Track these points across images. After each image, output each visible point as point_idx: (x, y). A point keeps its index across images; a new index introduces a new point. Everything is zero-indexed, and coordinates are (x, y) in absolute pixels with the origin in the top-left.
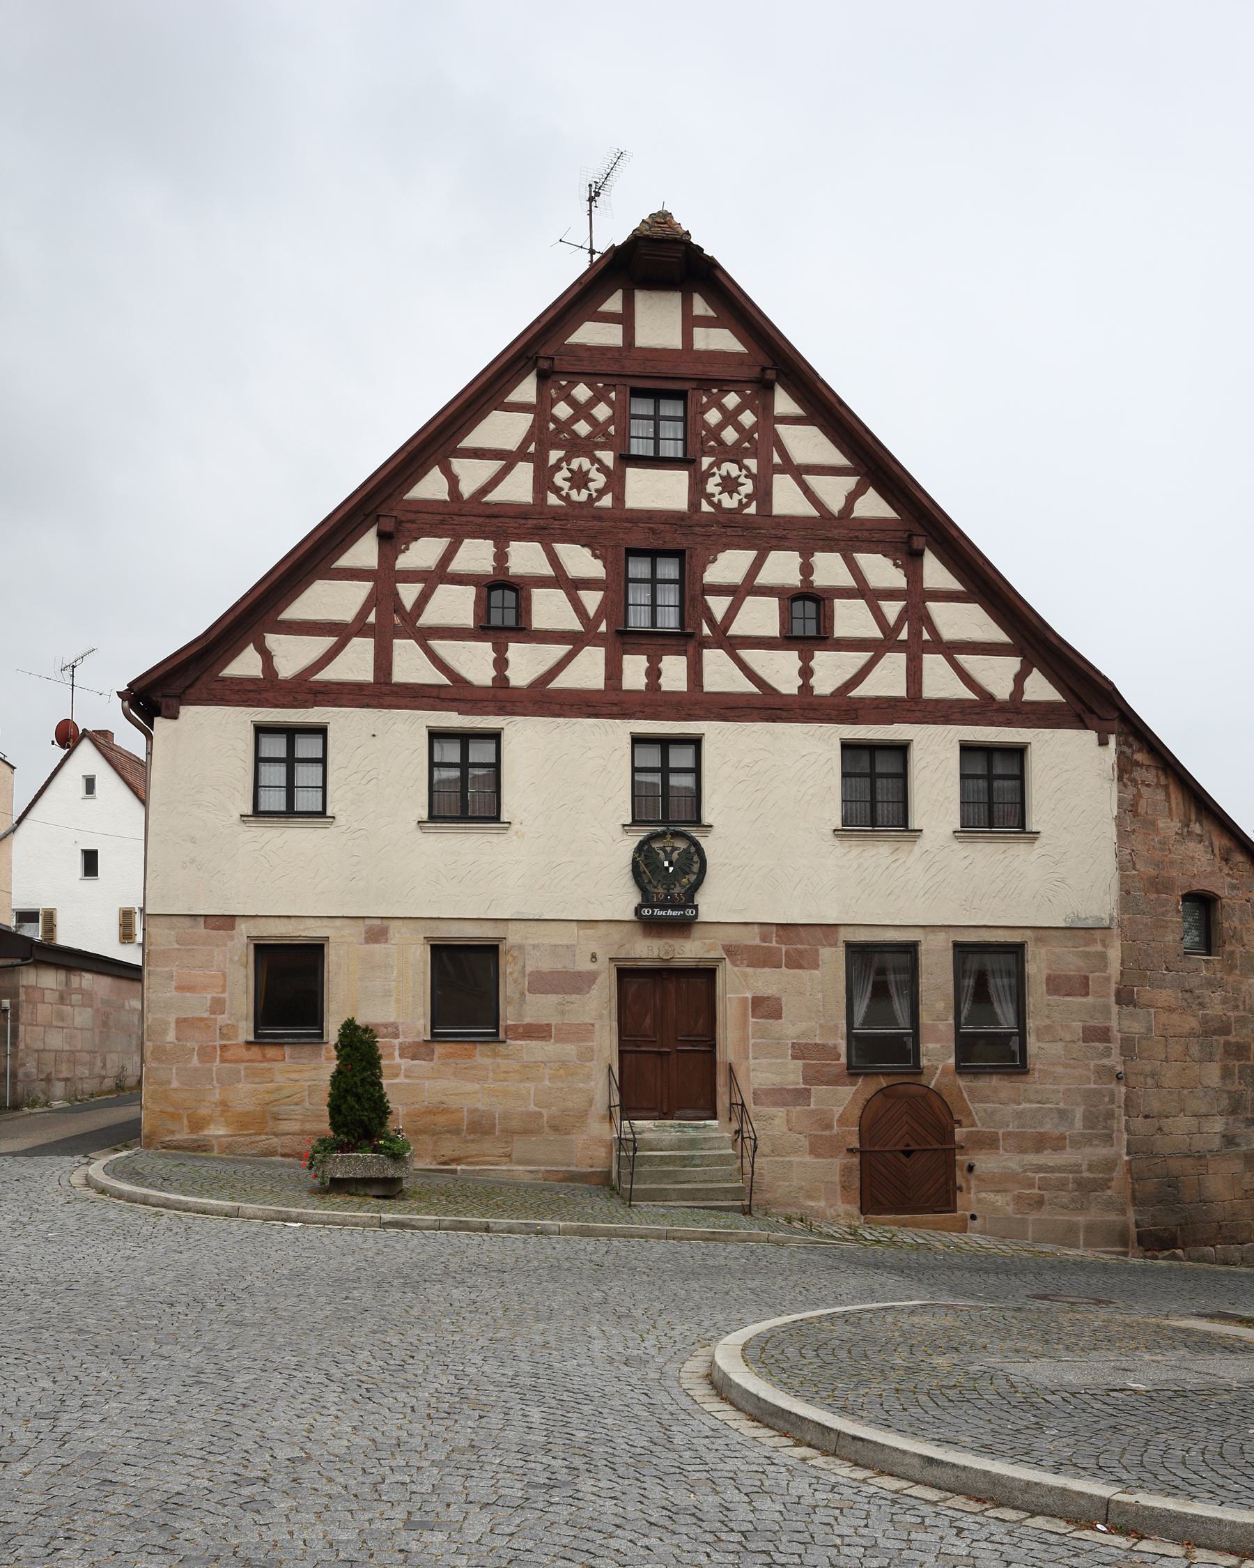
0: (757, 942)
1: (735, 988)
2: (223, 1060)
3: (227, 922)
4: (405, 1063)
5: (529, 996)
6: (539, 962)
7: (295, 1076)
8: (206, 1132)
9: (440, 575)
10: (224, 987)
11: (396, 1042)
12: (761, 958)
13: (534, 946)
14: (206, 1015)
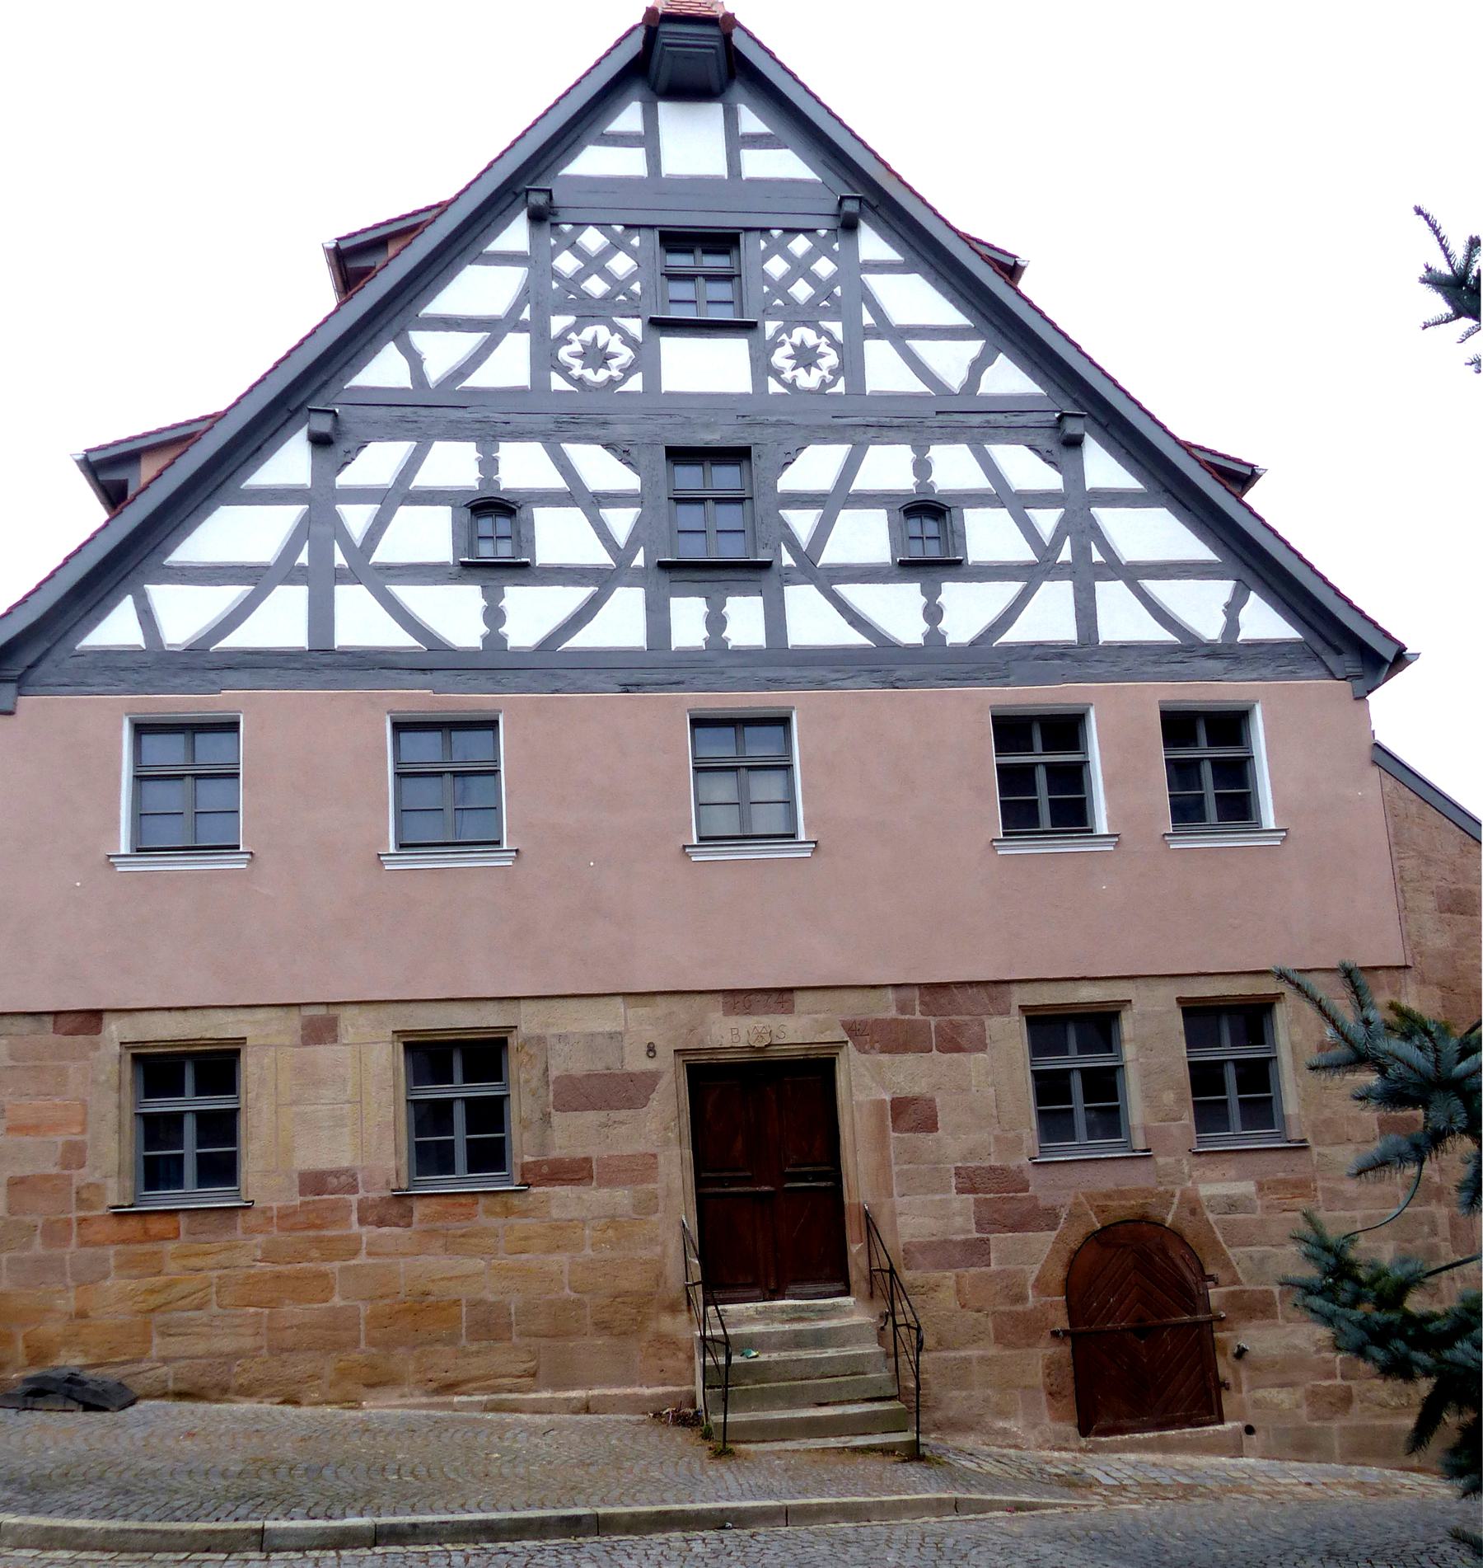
0: (893, 1013)
2: (84, 1243)
3: (92, 1019)
4: (368, 1233)
5: (557, 1118)
6: (567, 1063)
11: (353, 1199)
12: (895, 1039)
13: (560, 1037)
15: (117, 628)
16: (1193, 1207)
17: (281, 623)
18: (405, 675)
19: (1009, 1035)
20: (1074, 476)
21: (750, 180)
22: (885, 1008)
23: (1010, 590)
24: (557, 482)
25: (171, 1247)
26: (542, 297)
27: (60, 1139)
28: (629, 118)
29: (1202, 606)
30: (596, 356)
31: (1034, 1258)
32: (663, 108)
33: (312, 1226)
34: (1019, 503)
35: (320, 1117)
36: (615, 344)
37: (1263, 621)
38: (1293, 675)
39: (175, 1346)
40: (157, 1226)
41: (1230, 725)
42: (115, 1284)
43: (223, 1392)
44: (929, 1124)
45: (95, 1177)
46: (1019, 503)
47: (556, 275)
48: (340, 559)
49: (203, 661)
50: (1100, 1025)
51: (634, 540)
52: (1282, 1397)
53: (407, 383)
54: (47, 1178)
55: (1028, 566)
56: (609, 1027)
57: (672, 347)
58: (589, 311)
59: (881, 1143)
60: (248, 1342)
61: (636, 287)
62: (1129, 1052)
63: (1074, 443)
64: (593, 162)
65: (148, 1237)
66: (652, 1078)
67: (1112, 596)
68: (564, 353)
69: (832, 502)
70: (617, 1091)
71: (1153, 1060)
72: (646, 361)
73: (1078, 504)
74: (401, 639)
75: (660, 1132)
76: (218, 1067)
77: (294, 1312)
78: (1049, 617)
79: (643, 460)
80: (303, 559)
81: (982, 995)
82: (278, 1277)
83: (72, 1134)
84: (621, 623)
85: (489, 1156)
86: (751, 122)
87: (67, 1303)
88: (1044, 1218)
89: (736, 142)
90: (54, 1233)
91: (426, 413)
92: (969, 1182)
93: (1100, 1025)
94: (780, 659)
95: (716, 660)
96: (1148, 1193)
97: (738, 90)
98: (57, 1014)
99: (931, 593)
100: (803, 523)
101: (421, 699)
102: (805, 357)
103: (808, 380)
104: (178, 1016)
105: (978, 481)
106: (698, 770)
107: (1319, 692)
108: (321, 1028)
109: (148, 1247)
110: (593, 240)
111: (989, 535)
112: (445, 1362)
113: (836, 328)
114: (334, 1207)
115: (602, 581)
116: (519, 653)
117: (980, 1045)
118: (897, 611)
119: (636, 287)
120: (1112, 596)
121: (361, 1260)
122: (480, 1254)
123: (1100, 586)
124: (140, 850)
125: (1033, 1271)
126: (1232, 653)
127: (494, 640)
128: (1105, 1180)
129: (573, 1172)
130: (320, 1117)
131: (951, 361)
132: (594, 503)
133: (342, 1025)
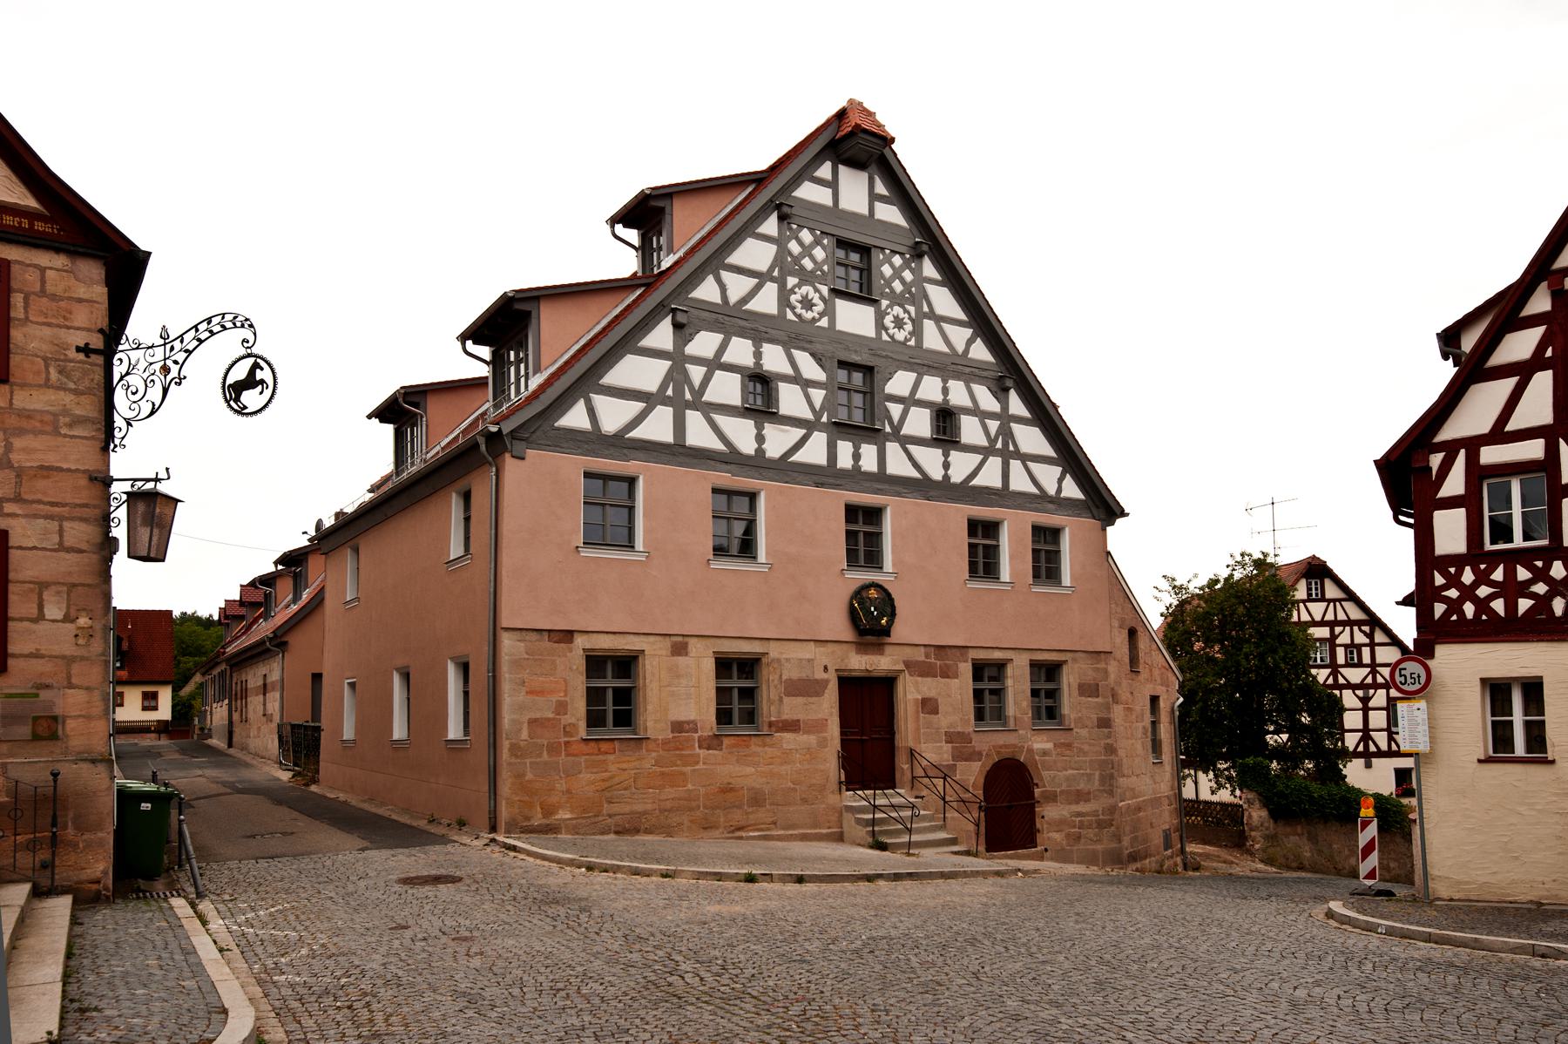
1: (910, 691)
2: (568, 755)
3: (568, 635)
4: (703, 753)
5: (786, 699)
7: (624, 766)
10: (566, 692)
12: (923, 670)
13: (788, 660)
15: (576, 418)
16: (1030, 751)
17: (658, 427)
19: (966, 669)
20: (1005, 407)
21: (879, 221)
22: (919, 655)
23: (799, 433)
24: (789, 371)
25: (611, 757)
26: (784, 266)
27: (554, 698)
28: (825, 171)
29: (1049, 476)
30: (807, 304)
31: (972, 774)
32: (841, 168)
34: (983, 416)
35: (679, 693)
36: (816, 300)
37: (1071, 490)
38: (1079, 515)
39: (616, 808)
40: (604, 746)
41: (1054, 534)
42: (586, 776)
43: (637, 831)
44: (935, 711)
45: (573, 720)
46: (983, 416)
47: (790, 254)
48: (688, 396)
49: (620, 444)
50: (1001, 666)
51: (823, 407)
52: (1057, 836)
53: (719, 301)
54: (549, 720)
55: (985, 448)
56: (808, 656)
57: (842, 306)
58: (806, 278)
59: (918, 718)
60: (649, 807)
61: (825, 268)
62: (1009, 682)
63: (1006, 390)
64: (809, 192)
65: (600, 752)
66: (827, 681)
67: (694, 419)
68: (793, 298)
69: (909, 401)
70: (806, 688)
71: (1017, 687)
72: (829, 312)
73: (1005, 418)
74: (718, 445)
75: (827, 707)
76: (626, 664)
77: (670, 792)
78: (990, 476)
79: (828, 365)
80: (670, 392)
81: (958, 653)
82: (663, 774)
83: (559, 696)
84: (815, 452)
85: (750, 717)
86: (881, 188)
87: (561, 785)
88: (973, 756)
89: (874, 197)
90: (553, 749)
91: (732, 320)
92: (951, 737)
93: (1001, 666)
94: (883, 480)
95: (854, 476)
96: (1015, 746)
97: (873, 167)
99: (760, 428)
100: (895, 410)
101: (726, 479)
102: (899, 323)
103: (900, 336)
104: (611, 637)
105: (968, 403)
107: (1088, 523)
108: (680, 649)
110: (806, 236)
111: (970, 431)
112: (737, 817)
113: (912, 309)
114: (688, 740)
115: (809, 426)
116: (771, 461)
117: (956, 676)
118: (931, 461)
119: (825, 268)
120: (694, 419)
121: (700, 766)
122: (741, 766)
123: (688, 412)
124: (630, 546)
125: (972, 779)
126: (1059, 503)
127: (760, 452)
128: (1002, 739)
129: (792, 726)
130: (679, 693)
131: (960, 336)
132: (806, 384)
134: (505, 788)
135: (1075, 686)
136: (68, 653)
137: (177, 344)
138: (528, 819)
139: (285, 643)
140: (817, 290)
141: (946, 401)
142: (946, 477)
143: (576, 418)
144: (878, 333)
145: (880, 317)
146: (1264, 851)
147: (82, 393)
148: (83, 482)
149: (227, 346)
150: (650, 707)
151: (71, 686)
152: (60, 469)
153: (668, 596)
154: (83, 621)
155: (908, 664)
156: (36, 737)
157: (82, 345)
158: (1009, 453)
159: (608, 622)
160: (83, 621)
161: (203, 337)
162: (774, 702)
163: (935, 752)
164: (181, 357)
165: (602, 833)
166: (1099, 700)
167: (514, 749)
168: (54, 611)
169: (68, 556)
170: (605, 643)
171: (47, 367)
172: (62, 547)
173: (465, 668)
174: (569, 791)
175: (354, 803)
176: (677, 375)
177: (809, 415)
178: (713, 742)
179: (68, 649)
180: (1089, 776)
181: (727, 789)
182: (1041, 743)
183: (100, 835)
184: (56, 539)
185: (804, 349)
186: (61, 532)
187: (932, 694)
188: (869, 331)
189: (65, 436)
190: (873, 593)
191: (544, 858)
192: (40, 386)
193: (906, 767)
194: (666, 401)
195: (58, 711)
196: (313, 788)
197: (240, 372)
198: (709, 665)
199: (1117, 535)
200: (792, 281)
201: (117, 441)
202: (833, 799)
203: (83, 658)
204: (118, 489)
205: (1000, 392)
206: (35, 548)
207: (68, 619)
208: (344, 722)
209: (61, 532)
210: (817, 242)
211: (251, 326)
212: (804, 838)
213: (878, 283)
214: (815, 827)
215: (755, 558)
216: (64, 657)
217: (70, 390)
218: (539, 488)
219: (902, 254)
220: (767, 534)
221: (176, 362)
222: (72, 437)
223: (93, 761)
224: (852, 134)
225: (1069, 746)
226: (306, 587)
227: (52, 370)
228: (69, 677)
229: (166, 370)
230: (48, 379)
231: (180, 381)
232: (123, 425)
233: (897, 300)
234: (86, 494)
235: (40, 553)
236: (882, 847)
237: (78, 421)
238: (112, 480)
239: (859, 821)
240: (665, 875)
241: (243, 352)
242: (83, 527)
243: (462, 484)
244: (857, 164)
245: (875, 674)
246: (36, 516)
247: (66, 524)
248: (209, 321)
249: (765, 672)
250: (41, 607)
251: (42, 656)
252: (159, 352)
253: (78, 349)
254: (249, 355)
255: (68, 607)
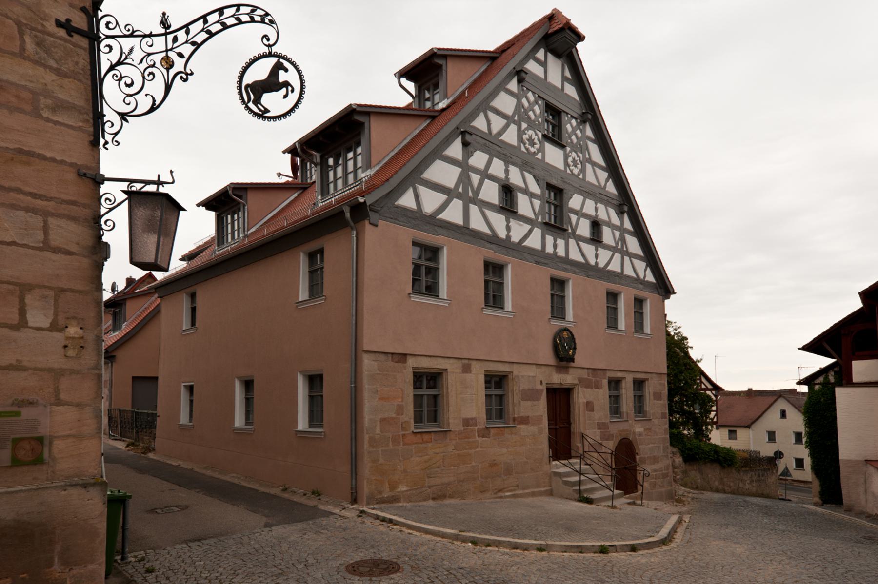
0: (586, 376)
1: (581, 397)
2: (404, 444)
3: (403, 357)
4: (480, 439)
5: (522, 403)
6: (524, 385)
7: (437, 451)
8: (399, 490)
9: (485, 175)
10: (402, 398)
11: (476, 428)
13: (523, 376)
14: (394, 416)
16: (634, 433)
18: (486, 243)
19: (605, 382)
25: (430, 445)
33: (467, 438)
36: (536, 141)
38: (652, 292)
40: (426, 437)
43: (444, 497)
44: (592, 410)
45: (406, 419)
48: (471, 194)
54: (393, 419)
56: (532, 374)
57: (549, 147)
58: (531, 125)
62: (624, 391)
63: (623, 213)
65: (424, 442)
66: (542, 391)
70: (530, 395)
72: (542, 150)
74: (487, 230)
75: (541, 408)
80: (460, 190)
82: (459, 455)
86: (568, 74)
98: (392, 354)
100: (574, 218)
103: (576, 171)
105: (606, 219)
106: (156, 378)
109: (424, 445)
113: (581, 155)
117: (601, 388)
122: (502, 449)
129: (525, 421)
130: (466, 399)
131: (603, 175)
132: (532, 195)
133: (473, 366)
134: (366, 469)
135: (652, 394)
136: (56, 366)
137: (182, 36)
138: (380, 493)
139: (114, 357)
140: (536, 134)
141: (597, 216)
142: (597, 263)
143: (407, 200)
144: (565, 168)
145: (566, 157)
146: (682, 480)
147: (66, 76)
148: (71, 176)
149: (246, 40)
150: (451, 409)
151: (59, 402)
152: (44, 158)
153: (453, 331)
154: (73, 331)
155: (580, 380)
156: (16, 462)
157: (63, 19)
158: (625, 253)
159: (427, 349)
160: (73, 331)
161: (214, 28)
162: (519, 407)
163: (593, 434)
164: (187, 50)
165: (425, 500)
166: (662, 402)
167: (371, 439)
168: (38, 317)
169: (54, 257)
170: (425, 364)
171: (21, 34)
172: (46, 246)
173: (315, 381)
174: (405, 471)
175: (196, 470)
176: (464, 179)
177: (532, 216)
178: (485, 432)
179: (56, 361)
180: (659, 447)
181: (493, 464)
182: (639, 429)
183: (91, 567)
184: (41, 237)
185: (530, 173)
186: (46, 229)
187: (591, 399)
188: (561, 166)
189: (48, 120)
190: (565, 335)
191: (427, 532)
192: (13, 54)
193: (580, 445)
194: (459, 196)
195: (43, 431)
196: (151, 455)
197: (260, 72)
198: (482, 379)
199: (670, 305)
200: (524, 126)
201: (108, 138)
202: (546, 467)
203: (73, 372)
204: (112, 191)
205: (620, 213)
206: (14, 243)
207: (54, 327)
208: (175, 410)
209: (46, 229)
210: (536, 102)
211: (272, 22)
212: (533, 494)
213: (565, 136)
214: (538, 487)
215: (503, 308)
216: (50, 370)
217: (51, 68)
218: (384, 250)
219: (576, 119)
220: (512, 293)
221: (181, 55)
222: (56, 123)
223: (85, 486)
224: (562, 30)
225: (649, 429)
226: (125, 321)
227: (27, 39)
228: (57, 392)
229: (168, 64)
230: (23, 49)
231: (186, 76)
232: (117, 120)
233: (574, 149)
234: (74, 190)
235: (21, 250)
236: (589, 501)
237: (60, 106)
238: (103, 180)
239: (566, 483)
240: (540, 549)
241: (266, 50)
242: (72, 226)
243: (313, 246)
244: (558, 55)
245: (564, 386)
246: (14, 207)
247: (51, 221)
248: (221, 11)
249: (510, 384)
250: (22, 312)
251: (25, 369)
252: (159, 44)
253: (59, 24)
254: (270, 55)
255: (56, 314)
